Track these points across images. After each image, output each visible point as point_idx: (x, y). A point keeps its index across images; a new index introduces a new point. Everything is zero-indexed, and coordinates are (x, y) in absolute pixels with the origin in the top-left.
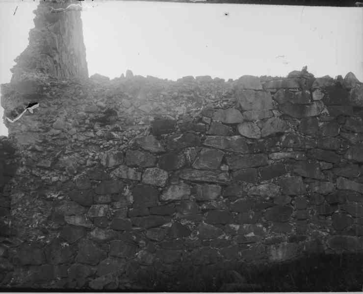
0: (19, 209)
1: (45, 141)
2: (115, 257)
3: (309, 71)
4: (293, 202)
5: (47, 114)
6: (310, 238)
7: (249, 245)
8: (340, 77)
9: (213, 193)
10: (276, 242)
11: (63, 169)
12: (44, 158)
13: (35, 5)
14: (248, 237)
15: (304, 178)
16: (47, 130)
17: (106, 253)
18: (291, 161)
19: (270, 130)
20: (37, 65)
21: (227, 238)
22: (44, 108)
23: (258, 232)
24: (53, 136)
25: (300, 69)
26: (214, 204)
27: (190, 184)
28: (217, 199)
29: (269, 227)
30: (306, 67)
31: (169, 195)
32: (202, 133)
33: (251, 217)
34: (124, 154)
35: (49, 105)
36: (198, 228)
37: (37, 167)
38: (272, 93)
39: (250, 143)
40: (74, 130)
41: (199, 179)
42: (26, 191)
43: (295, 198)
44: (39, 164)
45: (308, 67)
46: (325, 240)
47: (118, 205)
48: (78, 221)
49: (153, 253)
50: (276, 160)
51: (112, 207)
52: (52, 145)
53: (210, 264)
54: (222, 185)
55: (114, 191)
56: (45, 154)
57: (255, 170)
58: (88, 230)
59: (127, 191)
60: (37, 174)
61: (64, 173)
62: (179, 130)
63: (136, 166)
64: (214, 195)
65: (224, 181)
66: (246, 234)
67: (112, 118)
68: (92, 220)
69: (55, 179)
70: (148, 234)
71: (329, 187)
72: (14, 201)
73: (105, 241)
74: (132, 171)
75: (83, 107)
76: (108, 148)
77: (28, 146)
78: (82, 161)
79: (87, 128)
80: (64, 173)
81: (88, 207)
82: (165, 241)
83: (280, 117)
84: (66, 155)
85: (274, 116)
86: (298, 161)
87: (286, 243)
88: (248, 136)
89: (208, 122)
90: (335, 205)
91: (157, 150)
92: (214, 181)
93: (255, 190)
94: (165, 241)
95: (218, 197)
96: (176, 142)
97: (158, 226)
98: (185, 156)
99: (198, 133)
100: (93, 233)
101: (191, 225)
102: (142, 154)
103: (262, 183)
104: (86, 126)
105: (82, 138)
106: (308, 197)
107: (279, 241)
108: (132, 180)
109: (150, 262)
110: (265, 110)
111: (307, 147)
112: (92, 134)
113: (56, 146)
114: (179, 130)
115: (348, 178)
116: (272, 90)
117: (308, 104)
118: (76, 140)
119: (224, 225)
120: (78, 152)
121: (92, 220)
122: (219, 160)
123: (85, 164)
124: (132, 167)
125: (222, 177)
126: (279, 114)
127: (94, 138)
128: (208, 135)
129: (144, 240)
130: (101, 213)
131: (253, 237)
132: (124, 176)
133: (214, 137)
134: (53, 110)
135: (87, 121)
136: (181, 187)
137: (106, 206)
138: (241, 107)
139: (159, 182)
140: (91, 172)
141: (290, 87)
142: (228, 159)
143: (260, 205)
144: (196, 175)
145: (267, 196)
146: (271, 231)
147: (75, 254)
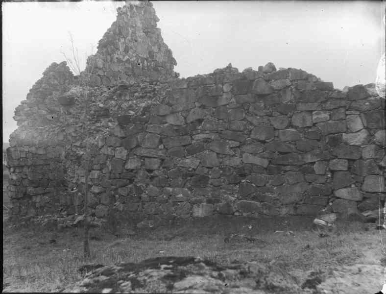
3: (233, 66)
6: (223, 201)
7: (179, 203)
8: (249, 71)
9: (155, 164)
14: (178, 197)
15: (218, 154)
16: (77, 123)
18: (207, 141)
19: (192, 118)
23: (185, 194)
26: (156, 172)
28: (158, 169)
30: (230, 64)
31: (130, 166)
33: (180, 183)
37: (75, 146)
39: (175, 128)
41: (145, 155)
50: (197, 140)
54: (161, 159)
55: (101, 162)
56: (78, 138)
57: (182, 148)
60: (75, 150)
63: (111, 146)
64: (156, 167)
65: (161, 156)
66: (178, 195)
71: (236, 161)
73: (98, 194)
74: (110, 149)
85: (195, 107)
87: (205, 204)
88: (173, 123)
90: (243, 176)
92: (155, 156)
93: (182, 163)
95: (159, 167)
97: (125, 186)
98: (137, 139)
101: (143, 186)
103: (187, 157)
107: (201, 202)
108: (110, 155)
111: (220, 129)
115: (252, 154)
116: (194, 87)
117: (221, 96)
119: (163, 187)
122: (157, 141)
124: (110, 146)
125: (160, 153)
126: (199, 105)
130: (96, 176)
131: (182, 197)
132: (106, 153)
133: (152, 125)
136: (135, 160)
137: (98, 172)
139: (123, 157)
142: (164, 140)
143: (188, 175)
144: (143, 152)
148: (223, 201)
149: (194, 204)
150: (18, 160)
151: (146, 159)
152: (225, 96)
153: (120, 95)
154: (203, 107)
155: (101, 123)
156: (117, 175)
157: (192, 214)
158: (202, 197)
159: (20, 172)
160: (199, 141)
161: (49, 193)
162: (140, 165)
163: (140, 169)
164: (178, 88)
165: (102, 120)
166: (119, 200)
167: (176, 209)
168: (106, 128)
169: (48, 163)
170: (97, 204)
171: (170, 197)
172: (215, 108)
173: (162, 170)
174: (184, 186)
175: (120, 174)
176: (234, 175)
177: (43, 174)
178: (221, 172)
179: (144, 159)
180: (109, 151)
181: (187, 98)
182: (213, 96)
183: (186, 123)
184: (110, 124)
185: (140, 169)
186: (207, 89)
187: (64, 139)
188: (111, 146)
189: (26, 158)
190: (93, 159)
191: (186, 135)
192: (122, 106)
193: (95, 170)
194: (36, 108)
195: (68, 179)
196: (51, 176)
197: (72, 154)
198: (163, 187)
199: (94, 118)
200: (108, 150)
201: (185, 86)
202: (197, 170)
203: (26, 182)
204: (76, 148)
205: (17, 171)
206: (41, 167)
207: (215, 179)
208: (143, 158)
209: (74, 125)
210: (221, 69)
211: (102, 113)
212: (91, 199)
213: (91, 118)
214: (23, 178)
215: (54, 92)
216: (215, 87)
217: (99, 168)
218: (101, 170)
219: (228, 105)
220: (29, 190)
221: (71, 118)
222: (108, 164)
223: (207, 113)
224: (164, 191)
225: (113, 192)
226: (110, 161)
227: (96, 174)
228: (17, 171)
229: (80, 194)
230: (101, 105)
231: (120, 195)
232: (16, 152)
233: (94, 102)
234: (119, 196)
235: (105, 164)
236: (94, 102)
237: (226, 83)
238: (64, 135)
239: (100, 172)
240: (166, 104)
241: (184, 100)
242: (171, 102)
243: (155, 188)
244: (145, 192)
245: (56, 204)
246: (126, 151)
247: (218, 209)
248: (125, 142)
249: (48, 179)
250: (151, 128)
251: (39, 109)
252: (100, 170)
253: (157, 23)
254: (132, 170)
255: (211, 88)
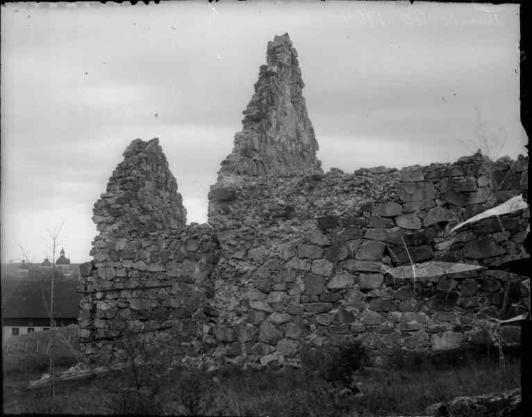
0: (220, 293)
1: (238, 237)
2: (290, 338)
4: (460, 287)
5: (239, 213)
6: (476, 328)
7: (411, 333)
10: (440, 331)
11: (252, 260)
12: (238, 250)
13: (407, 98)
16: (239, 227)
17: (282, 335)
19: (432, 219)
20: (236, 169)
21: (389, 325)
22: (236, 208)
24: (243, 232)
25: (470, 153)
26: (377, 292)
27: (353, 274)
29: (433, 316)
30: (480, 150)
31: (336, 283)
32: (363, 226)
33: (413, 305)
34: (297, 247)
35: (240, 206)
36: (362, 314)
37: (233, 258)
38: (435, 183)
39: (409, 233)
40: (260, 226)
42: (225, 279)
43: (464, 282)
44: (233, 256)
45: (482, 150)
46: (493, 331)
47: (291, 292)
48: (259, 305)
49: (322, 336)
51: (288, 294)
52: (243, 239)
53: (373, 349)
55: (288, 279)
58: (268, 314)
59: (299, 280)
61: (254, 263)
62: (342, 225)
64: (376, 284)
66: (409, 321)
67: (292, 213)
68: (271, 305)
69: (246, 268)
70: (318, 318)
72: (217, 287)
73: (282, 324)
74: (303, 262)
75: (267, 206)
76: (288, 240)
77: (226, 241)
78: (266, 253)
79: (271, 224)
80: (254, 263)
81: (268, 293)
82: (332, 326)
83: (443, 206)
84: (254, 247)
85: (436, 205)
86: (467, 242)
87: (450, 332)
89: (368, 216)
91: (323, 244)
94: (332, 326)
95: (381, 285)
96: (339, 236)
97: (325, 312)
99: (359, 227)
100: (271, 316)
102: (310, 247)
104: (270, 222)
105: (267, 233)
106: (481, 282)
107: (443, 330)
108: (303, 271)
109: (320, 344)
110: (427, 200)
112: (275, 229)
113: (247, 240)
114: (342, 225)
116: (435, 180)
117: (474, 191)
118: (261, 235)
120: (264, 245)
121: (271, 305)
123: (269, 255)
124: (303, 258)
127: (277, 232)
128: (368, 228)
129: (315, 324)
132: (296, 267)
134: (243, 209)
135: (271, 218)
137: (282, 293)
138: (400, 200)
140: (270, 263)
141: (454, 175)
144: (358, 265)
145: (430, 282)
146: (434, 320)
147: (257, 334)
148: (476, 328)
149: (434, 333)
150: (112, 280)
151: (361, 275)
152: (480, 192)
153: (311, 188)
154: (447, 206)
155: (278, 226)
156: (315, 298)
157: (431, 347)
158: (447, 324)
159: (116, 299)
160: (445, 251)
161: (168, 328)
162: (352, 282)
163: (352, 288)
164: (412, 180)
165: (279, 222)
166: (315, 332)
167: (407, 341)
168: (289, 233)
169: (169, 285)
170: (279, 338)
171: (397, 325)
172: (464, 207)
173: (387, 289)
174: (419, 309)
175: (319, 295)
176: (500, 292)
177: (160, 301)
178: (479, 286)
179: (358, 275)
180: (302, 265)
181: (424, 193)
182: (463, 192)
183: (423, 227)
184: (294, 228)
185: (352, 288)
186: (454, 183)
187: (198, 249)
188: (307, 258)
189: (125, 277)
190: (273, 276)
191: (424, 243)
192: (315, 203)
193: (277, 291)
194: (128, 205)
195: (220, 305)
196: (173, 303)
197: (228, 270)
198: (386, 312)
199: (269, 220)
200: (299, 263)
201: (422, 178)
202: (440, 284)
203: (126, 313)
204: (235, 262)
205: (109, 296)
206: (155, 290)
207: (44, 322)
208: (357, 273)
209: (233, 229)
210: (469, 157)
211: (281, 212)
212: (267, 331)
213: (263, 219)
214: (120, 308)
215: (147, 183)
216: (465, 180)
217: (285, 289)
218: (286, 291)
219: (485, 203)
220: (132, 325)
221: (230, 219)
222: (299, 282)
223: (454, 213)
224: (390, 317)
225: (306, 321)
226: (302, 278)
227: (278, 297)
228: (109, 296)
229: (249, 325)
230: (282, 202)
231: (318, 325)
232: (109, 269)
233: (268, 197)
234: (317, 327)
235: (293, 282)
236: (268, 197)
237: (481, 175)
238: (198, 245)
239: (285, 293)
240: (397, 202)
241: (420, 196)
242: (402, 198)
243: (375, 313)
244: (359, 319)
245: (183, 344)
246: (331, 264)
247: (470, 339)
248: (330, 251)
249: (168, 308)
250: (370, 233)
251: (131, 206)
252: (285, 291)
253: (303, 90)
254: (337, 290)
255: (461, 181)
